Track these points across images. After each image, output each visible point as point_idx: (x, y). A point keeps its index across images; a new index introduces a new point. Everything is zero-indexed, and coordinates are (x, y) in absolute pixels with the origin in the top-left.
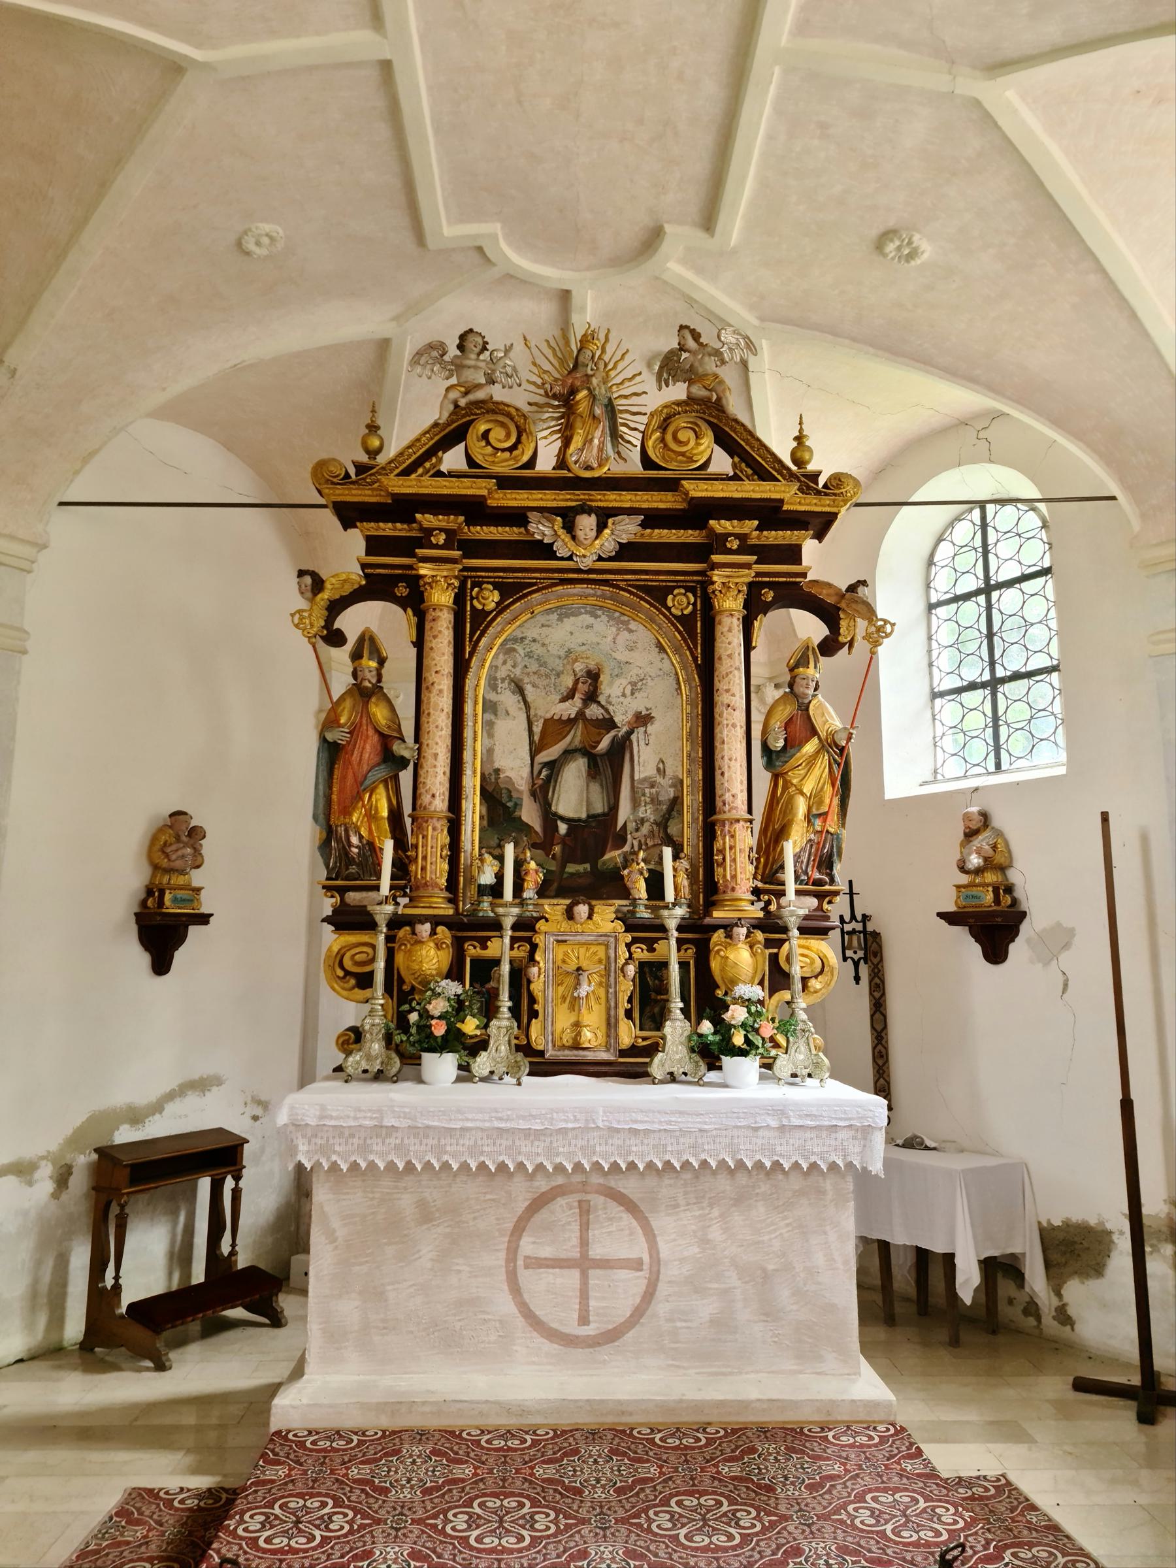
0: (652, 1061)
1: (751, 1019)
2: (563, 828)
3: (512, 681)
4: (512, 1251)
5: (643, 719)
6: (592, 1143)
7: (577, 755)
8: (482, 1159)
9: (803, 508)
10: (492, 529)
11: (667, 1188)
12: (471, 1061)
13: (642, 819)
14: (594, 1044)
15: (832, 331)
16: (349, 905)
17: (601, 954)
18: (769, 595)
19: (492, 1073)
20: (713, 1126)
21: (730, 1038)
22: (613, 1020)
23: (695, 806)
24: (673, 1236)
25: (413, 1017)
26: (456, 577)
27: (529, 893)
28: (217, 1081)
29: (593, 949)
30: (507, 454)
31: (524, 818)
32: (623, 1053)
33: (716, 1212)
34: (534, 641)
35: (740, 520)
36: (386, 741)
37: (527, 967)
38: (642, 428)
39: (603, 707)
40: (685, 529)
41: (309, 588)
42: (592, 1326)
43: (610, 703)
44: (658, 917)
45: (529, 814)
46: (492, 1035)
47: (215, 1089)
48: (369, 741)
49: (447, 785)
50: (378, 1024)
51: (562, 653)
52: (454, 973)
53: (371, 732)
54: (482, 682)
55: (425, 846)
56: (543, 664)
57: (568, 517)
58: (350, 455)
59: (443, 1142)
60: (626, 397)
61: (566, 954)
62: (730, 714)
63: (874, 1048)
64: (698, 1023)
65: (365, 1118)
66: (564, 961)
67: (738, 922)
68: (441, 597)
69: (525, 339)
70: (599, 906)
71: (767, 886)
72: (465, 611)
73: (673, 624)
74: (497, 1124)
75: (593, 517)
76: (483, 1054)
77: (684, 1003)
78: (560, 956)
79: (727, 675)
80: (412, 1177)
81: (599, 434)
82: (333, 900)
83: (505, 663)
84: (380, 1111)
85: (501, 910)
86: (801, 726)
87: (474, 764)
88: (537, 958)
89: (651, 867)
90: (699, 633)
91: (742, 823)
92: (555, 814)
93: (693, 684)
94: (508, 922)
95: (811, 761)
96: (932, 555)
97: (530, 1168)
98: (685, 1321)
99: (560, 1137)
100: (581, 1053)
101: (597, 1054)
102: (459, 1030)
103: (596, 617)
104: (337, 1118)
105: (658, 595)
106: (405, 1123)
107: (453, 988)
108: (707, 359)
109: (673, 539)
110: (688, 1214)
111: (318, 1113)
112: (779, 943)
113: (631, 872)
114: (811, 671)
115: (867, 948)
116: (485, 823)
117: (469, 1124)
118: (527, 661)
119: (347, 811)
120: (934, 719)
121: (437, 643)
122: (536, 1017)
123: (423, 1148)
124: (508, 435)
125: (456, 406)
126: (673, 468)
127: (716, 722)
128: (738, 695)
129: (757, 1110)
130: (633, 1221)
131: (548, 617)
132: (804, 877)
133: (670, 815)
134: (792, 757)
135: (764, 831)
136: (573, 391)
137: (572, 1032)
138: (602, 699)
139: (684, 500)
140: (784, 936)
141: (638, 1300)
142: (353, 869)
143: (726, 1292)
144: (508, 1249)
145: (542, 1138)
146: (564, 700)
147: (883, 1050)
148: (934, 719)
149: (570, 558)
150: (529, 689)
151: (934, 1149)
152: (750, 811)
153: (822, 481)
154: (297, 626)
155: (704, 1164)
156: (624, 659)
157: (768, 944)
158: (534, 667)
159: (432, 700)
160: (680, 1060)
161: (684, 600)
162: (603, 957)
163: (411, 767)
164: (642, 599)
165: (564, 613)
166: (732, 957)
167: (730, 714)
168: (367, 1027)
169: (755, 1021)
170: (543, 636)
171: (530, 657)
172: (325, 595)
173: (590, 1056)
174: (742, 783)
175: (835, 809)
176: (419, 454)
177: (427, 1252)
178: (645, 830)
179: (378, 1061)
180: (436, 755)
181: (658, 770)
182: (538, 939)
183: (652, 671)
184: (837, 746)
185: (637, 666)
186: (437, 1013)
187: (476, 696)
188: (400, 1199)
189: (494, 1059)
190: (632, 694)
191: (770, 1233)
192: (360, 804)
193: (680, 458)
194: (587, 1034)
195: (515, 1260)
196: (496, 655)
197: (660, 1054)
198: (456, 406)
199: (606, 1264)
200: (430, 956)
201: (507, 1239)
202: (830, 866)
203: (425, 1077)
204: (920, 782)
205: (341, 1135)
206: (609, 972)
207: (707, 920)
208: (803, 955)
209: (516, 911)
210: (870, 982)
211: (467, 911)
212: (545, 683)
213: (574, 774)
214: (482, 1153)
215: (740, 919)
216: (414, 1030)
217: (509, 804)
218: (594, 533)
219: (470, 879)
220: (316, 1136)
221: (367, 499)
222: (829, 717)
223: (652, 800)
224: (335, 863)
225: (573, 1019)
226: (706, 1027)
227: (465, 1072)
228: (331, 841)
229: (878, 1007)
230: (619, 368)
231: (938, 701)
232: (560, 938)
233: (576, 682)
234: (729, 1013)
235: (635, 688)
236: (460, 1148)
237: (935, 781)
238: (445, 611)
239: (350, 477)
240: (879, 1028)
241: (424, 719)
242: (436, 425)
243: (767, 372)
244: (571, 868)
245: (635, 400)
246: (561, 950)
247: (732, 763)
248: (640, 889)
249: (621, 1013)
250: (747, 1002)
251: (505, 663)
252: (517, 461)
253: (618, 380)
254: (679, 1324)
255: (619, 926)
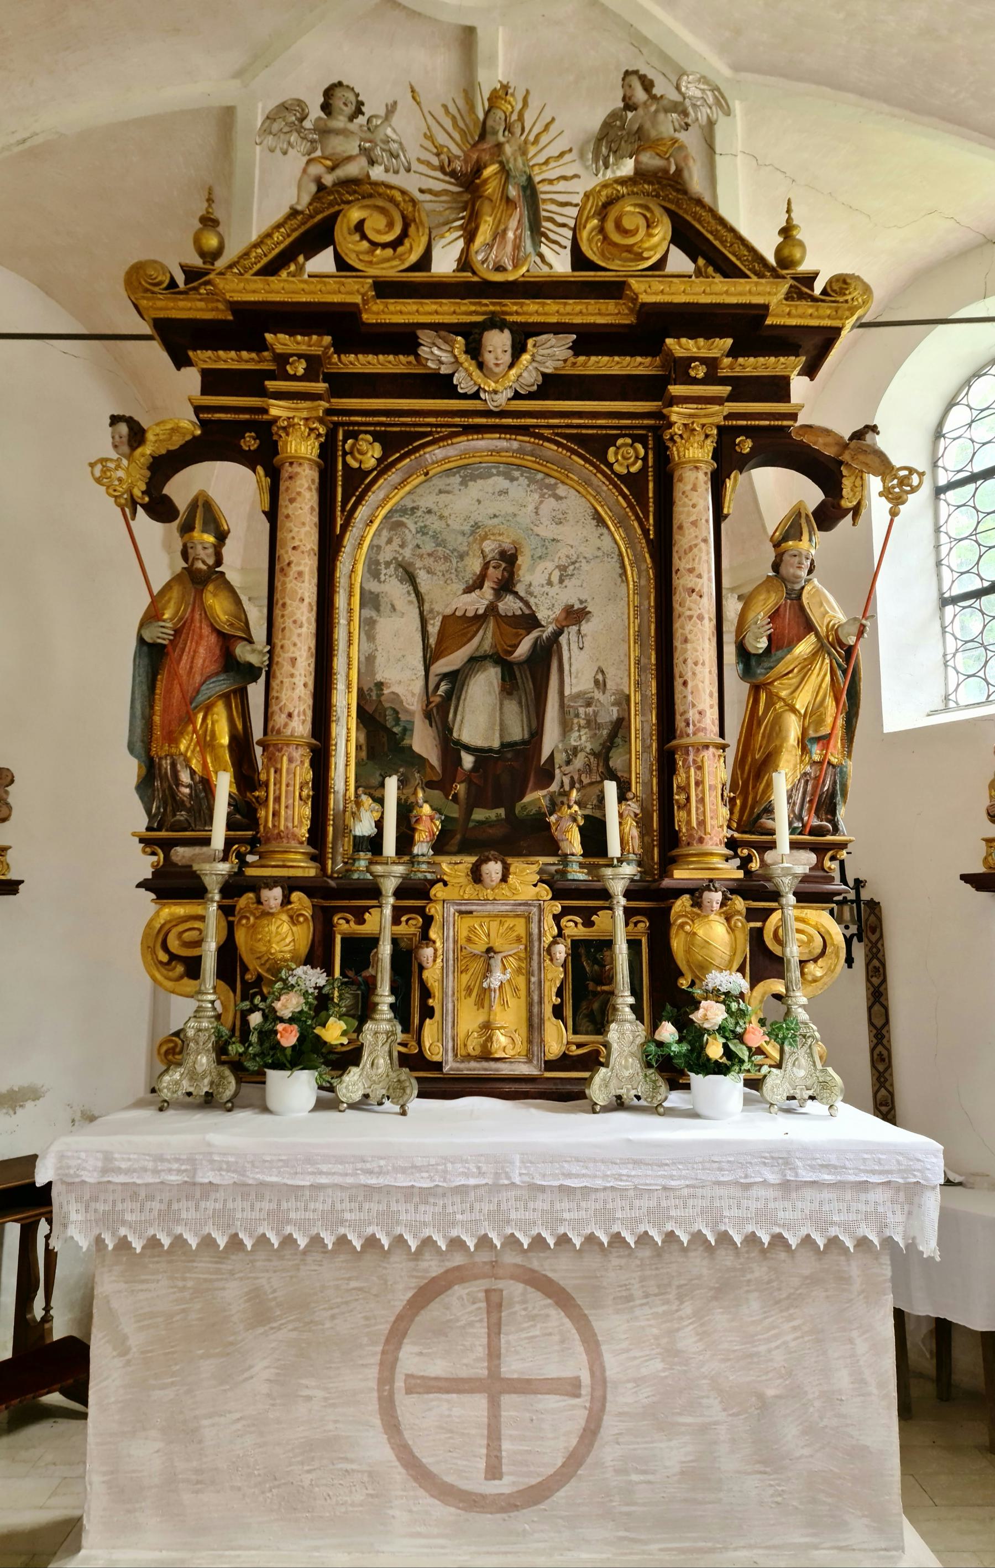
0: (591, 1078)
1: (732, 1021)
2: (468, 761)
3: (400, 565)
4: (388, 1365)
5: (575, 615)
6: (504, 1206)
7: (488, 663)
8: (342, 1231)
9: (793, 322)
10: (370, 357)
11: (615, 1273)
12: (335, 1082)
13: (575, 748)
14: (510, 1053)
15: (832, 81)
16: (176, 865)
17: (521, 929)
18: (746, 445)
19: (366, 1096)
20: (683, 1182)
21: (703, 1048)
22: (536, 1020)
23: (647, 729)
24: (625, 1345)
25: (255, 1019)
26: (321, 421)
27: (422, 847)
28: (31, 1094)
29: (510, 922)
30: (389, 252)
31: (416, 748)
32: (550, 1065)
33: (688, 1309)
34: (429, 512)
35: (707, 338)
36: (226, 641)
37: (418, 947)
38: (572, 223)
39: (521, 599)
40: (632, 355)
41: (125, 439)
42: (507, 1479)
43: (531, 594)
44: (600, 878)
45: (423, 742)
46: (366, 1044)
47: (30, 1104)
48: (204, 643)
49: (310, 702)
50: (206, 1030)
51: (467, 528)
52: (318, 955)
53: (206, 631)
54: (360, 568)
55: (278, 782)
56: (441, 543)
57: (472, 338)
58: (176, 256)
59: (285, 1205)
60: (551, 182)
61: (472, 930)
62: (695, 602)
63: (872, 1050)
64: (655, 1027)
65: (170, 1170)
66: (469, 940)
67: (710, 885)
68: (301, 447)
69: (413, 91)
70: (516, 865)
71: (747, 837)
72: (336, 471)
73: (616, 486)
74: (364, 1180)
75: (507, 332)
76: (354, 1070)
77: (632, 1002)
78: (464, 933)
79: (691, 549)
80: (241, 1255)
81: (515, 223)
82: (155, 858)
83: (389, 541)
84: (191, 1160)
85: (379, 869)
86: (793, 619)
87: (348, 676)
88: (433, 934)
89: (588, 812)
90: (652, 498)
91: (712, 750)
92: (458, 743)
93: (643, 567)
94: (389, 886)
95: (807, 664)
96: (940, 424)
97: (413, 1245)
98: (645, 1472)
99: (458, 1199)
100: (493, 1065)
101: (514, 1066)
102: (318, 1037)
103: (513, 479)
104: (128, 1172)
105: (594, 446)
106: (228, 1178)
107: (313, 978)
108: (661, 116)
109: (616, 371)
110: (647, 1310)
111: (100, 1164)
112: (765, 914)
113: (560, 819)
114: (804, 544)
115: (866, 923)
116: (364, 754)
117: (323, 1180)
118: (420, 539)
119: (172, 739)
120: (944, 632)
121: (295, 509)
122: (431, 1017)
123: (256, 1215)
124: (390, 225)
125: (321, 187)
126: (616, 268)
127: (675, 614)
128: (705, 576)
129: (749, 1158)
130: (566, 1320)
131: (448, 481)
132: (798, 824)
133: (612, 743)
134: (779, 661)
135: (740, 762)
136: (478, 169)
137: (480, 1036)
138: (520, 589)
139: (631, 310)
140: (774, 905)
141: (574, 1442)
142: (182, 816)
143: (704, 1429)
144: (382, 1364)
145: (432, 1200)
146: (469, 590)
147: (885, 1053)
148: (944, 632)
149: (476, 396)
150: (422, 576)
151: (960, 1184)
152: (722, 735)
153: (818, 287)
154: (98, 481)
155: (670, 1237)
156: (550, 535)
157: (752, 914)
158: (429, 546)
159: (289, 586)
160: (631, 1078)
161: (631, 451)
162: (523, 934)
163: (262, 679)
164: (574, 452)
165: (468, 472)
166: (700, 932)
167: (695, 602)
168: (191, 1033)
169: (737, 1023)
170: (441, 505)
171: (424, 534)
172: (147, 450)
173: (505, 1069)
174: (711, 695)
175: (839, 732)
176: (270, 256)
177: (262, 1369)
178: (579, 762)
179: (206, 1081)
180: (293, 661)
181: (596, 682)
182: (434, 910)
183: (588, 551)
184: (841, 644)
185: (567, 544)
186: (287, 1014)
187: (351, 586)
188: (224, 1289)
189: (369, 1077)
190: (561, 581)
191: (768, 1340)
192: (190, 728)
193: (625, 255)
194: (501, 1039)
195: (391, 1381)
196: (379, 531)
197: (603, 1070)
198: (321, 187)
199: (526, 1387)
200: (282, 933)
201: (379, 1348)
202: (832, 810)
203: (271, 1104)
204: (928, 711)
205: (134, 1196)
206: (532, 956)
207: (666, 883)
208: (798, 931)
209: (400, 869)
210: (867, 965)
211: (338, 872)
212: (443, 568)
213: (483, 689)
214: (342, 1222)
215: (711, 880)
216: (254, 1038)
217: (396, 730)
218: (507, 358)
219: (344, 830)
220: (96, 1199)
221: (199, 315)
222: (829, 609)
223: (589, 722)
224: (158, 808)
225: (481, 1019)
226: (668, 1032)
227: (328, 1101)
228: (154, 780)
229: (878, 996)
230: (544, 139)
231: (949, 610)
232: (463, 908)
233: (486, 566)
234: (701, 1012)
235: (564, 573)
236: (310, 1215)
237: (946, 709)
238: (306, 465)
239: (177, 286)
240: (879, 1023)
241: (277, 612)
242: (294, 213)
243: (740, 156)
244: (480, 814)
245: (561, 186)
246: (464, 925)
247: (699, 669)
248: (573, 842)
249: (548, 1011)
250: (726, 997)
251: (389, 541)
252: (403, 261)
253: (541, 159)
254: (635, 1477)
255: (544, 892)
